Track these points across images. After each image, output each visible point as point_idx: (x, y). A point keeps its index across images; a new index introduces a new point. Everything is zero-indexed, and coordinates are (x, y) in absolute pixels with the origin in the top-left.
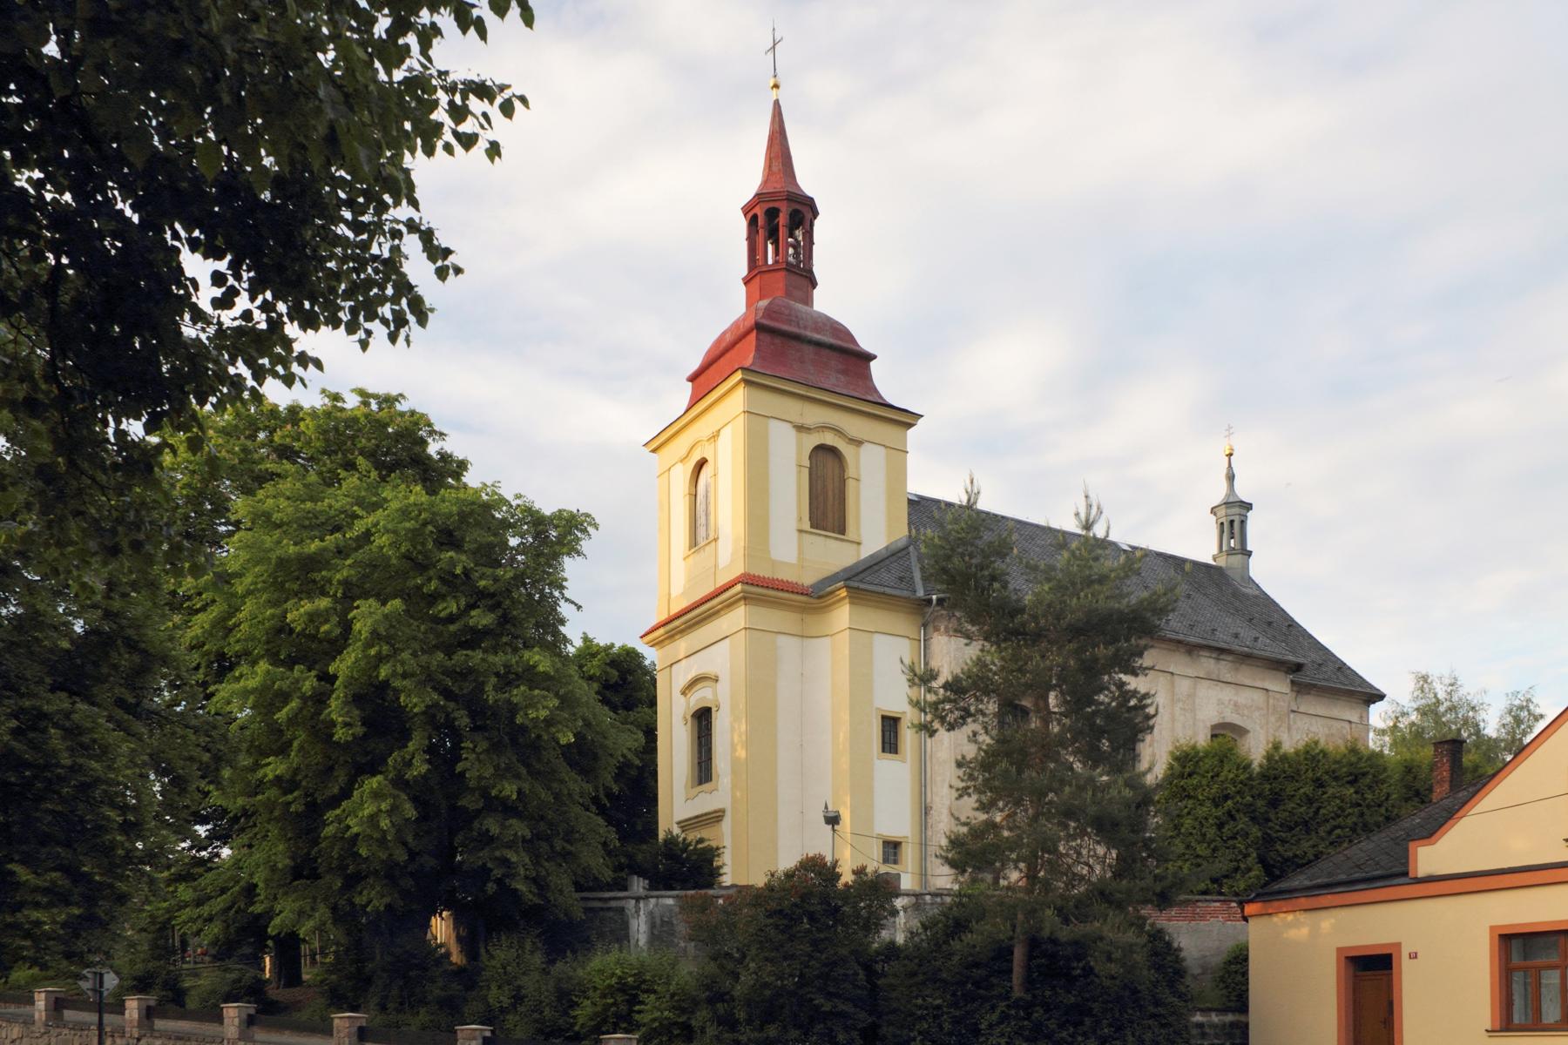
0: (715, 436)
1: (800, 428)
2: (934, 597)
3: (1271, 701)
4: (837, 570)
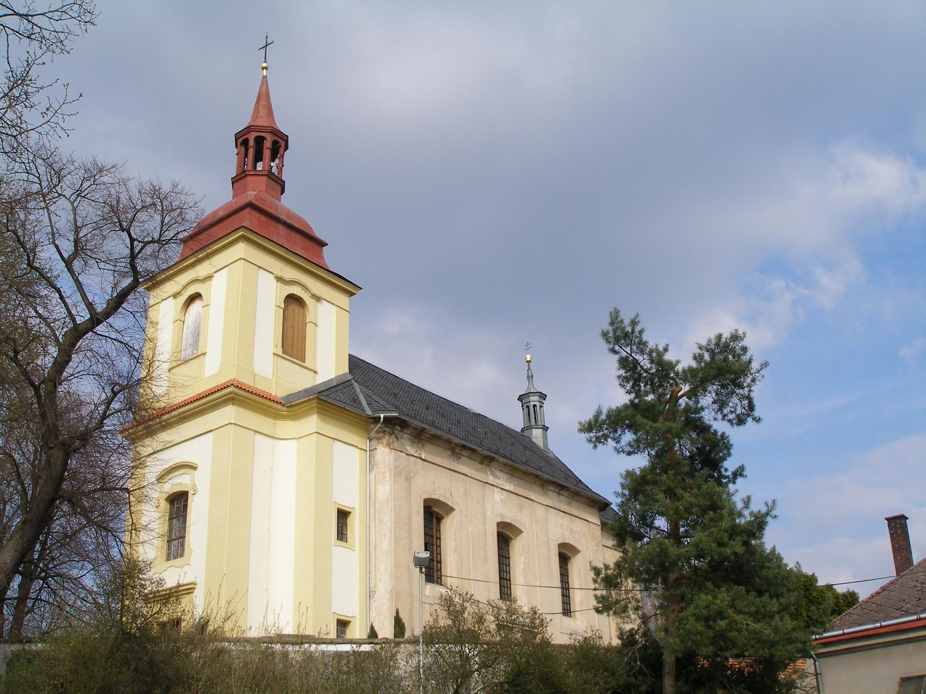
0: (209, 278)
1: (279, 279)
2: (382, 416)
3: (591, 530)
4: (300, 389)
